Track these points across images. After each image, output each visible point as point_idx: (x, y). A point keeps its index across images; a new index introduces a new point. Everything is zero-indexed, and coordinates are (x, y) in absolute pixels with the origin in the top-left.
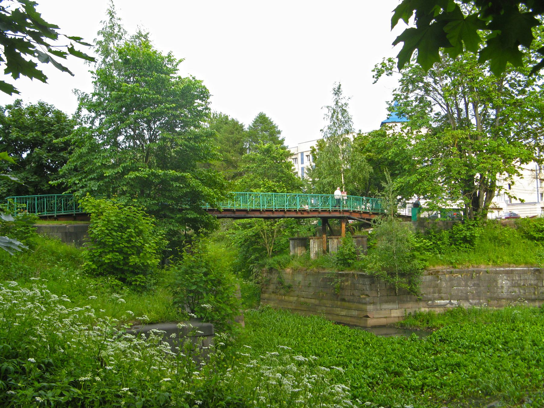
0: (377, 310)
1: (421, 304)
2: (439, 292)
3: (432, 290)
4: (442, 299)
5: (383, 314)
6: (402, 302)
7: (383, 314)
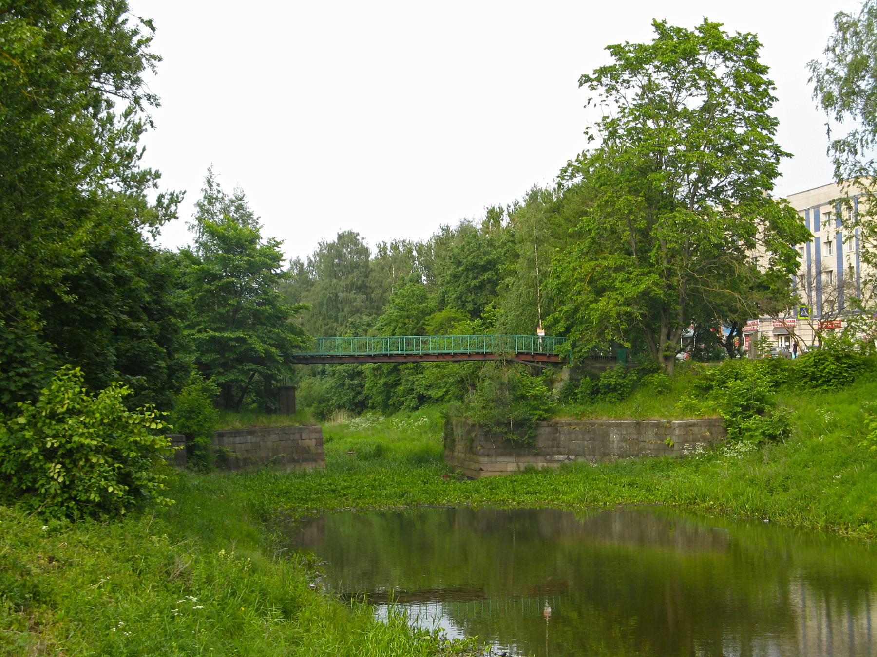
0: (492, 462)
1: (540, 458)
2: (558, 447)
3: (550, 443)
4: (560, 453)
5: (499, 467)
6: (519, 455)
7: (499, 467)
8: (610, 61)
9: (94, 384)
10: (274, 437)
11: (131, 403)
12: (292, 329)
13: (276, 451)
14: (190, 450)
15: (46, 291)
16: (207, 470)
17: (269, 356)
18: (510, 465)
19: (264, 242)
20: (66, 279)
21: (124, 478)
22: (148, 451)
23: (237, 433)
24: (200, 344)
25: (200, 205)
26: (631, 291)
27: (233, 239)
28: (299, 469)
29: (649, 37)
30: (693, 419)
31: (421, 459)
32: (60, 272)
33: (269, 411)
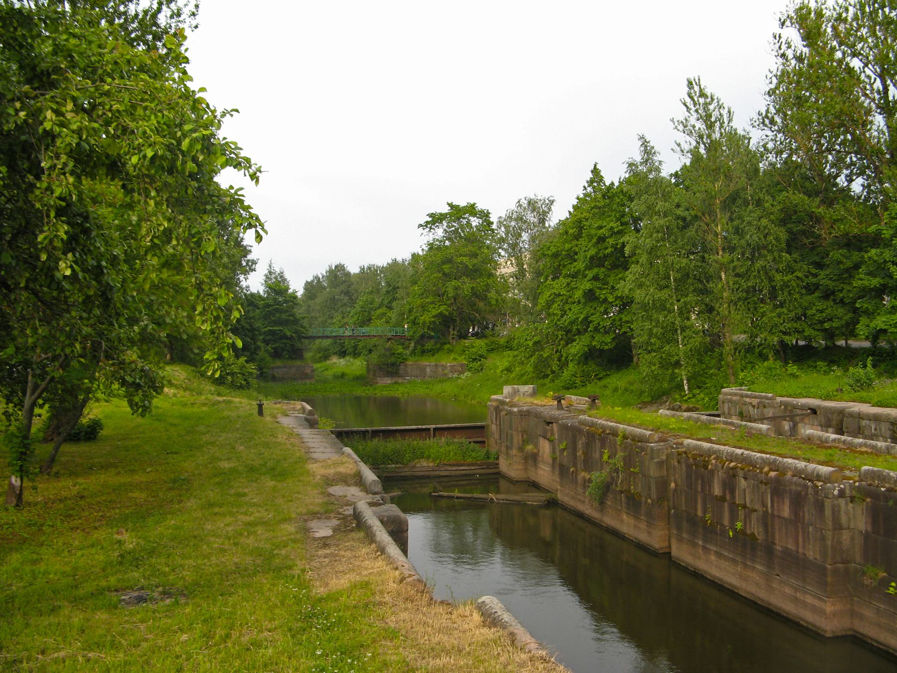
14: (261, 374)
16: (267, 381)
17: (292, 336)
18: (389, 381)
19: (290, 291)
21: (245, 380)
22: (251, 373)
23: (279, 367)
24: (265, 332)
25: (266, 275)
26: (434, 312)
29: (446, 209)
30: (455, 363)
31: (357, 378)
33: (292, 358)
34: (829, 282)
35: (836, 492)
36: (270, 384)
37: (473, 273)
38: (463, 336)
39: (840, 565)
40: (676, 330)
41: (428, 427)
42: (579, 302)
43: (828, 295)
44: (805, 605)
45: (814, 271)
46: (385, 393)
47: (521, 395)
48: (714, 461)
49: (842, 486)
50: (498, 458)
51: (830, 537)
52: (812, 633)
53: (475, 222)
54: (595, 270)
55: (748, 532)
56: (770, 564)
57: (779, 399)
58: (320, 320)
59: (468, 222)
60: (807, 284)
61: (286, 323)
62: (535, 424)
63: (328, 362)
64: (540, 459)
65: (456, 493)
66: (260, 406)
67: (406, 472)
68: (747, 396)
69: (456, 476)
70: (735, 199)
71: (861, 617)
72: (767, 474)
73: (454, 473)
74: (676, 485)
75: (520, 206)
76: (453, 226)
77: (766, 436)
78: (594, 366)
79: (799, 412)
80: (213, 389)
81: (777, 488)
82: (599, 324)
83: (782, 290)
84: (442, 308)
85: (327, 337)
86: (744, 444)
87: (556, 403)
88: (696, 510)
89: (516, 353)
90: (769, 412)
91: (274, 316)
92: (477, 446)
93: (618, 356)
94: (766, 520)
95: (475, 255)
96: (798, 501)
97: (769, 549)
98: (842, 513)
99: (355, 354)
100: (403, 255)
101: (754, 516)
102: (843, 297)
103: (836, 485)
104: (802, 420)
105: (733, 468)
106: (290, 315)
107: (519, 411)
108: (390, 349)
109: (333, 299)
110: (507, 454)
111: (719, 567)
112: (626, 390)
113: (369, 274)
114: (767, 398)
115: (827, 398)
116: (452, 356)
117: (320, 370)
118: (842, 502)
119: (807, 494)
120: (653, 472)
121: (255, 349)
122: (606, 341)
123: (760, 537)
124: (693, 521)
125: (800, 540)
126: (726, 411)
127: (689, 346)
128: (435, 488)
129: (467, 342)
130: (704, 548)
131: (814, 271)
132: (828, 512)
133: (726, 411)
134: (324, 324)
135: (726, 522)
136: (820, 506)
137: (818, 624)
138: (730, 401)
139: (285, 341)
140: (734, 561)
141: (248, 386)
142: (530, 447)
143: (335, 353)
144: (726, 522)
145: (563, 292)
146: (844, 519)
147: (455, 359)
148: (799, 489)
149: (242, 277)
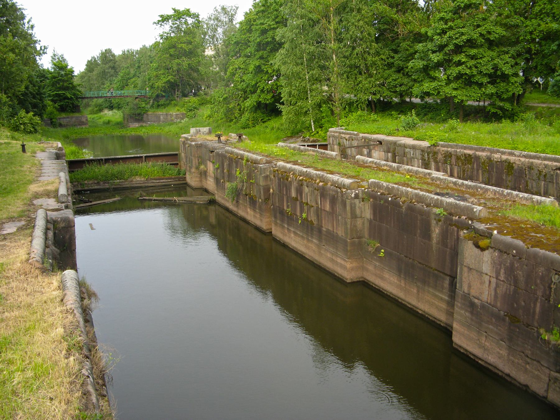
8: (160, 19)
9: (27, 112)
10: (74, 119)
11: (34, 115)
12: (78, 90)
13: (75, 122)
15: (17, 96)
17: (71, 98)
18: (137, 125)
19: (69, 67)
20: (21, 94)
21: (33, 128)
23: (64, 118)
24: (53, 95)
26: (165, 80)
27: (61, 66)
28: (81, 127)
29: (171, 12)
30: (178, 113)
32: (20, 93)
33: (73, 112)
34: (400, 62)
35: (353, 195)
36: (59, 129)
37: (190, 54)
38: (185, 95)
39: (356, 240)
40: (307, 92)
41: (141, 155)
42: (251, 73)
43: (400, 70)
44: (337, 263)
45: (392, 54)
46: (133, 133)
47: (200, 134)
48: (291, 176)
49: (357, 192)
50: (185, 174)
51: (349, 223)
52: (339, 280)
53: (190, 21)
54: (261, 53)
55: (309, 220)
56: (320, 239)
57: (361, 135)
58: (96, 85)
59: (186, 21)
60: (388, 63)
61: (67, 89)
62: (204, 152)
63: (102, 113)
64: (208, 174)
65: (154, 197)
66: (23, 146)
67: (127, 184)
68: (343, 133)
69: (159, 186)
70: (345, 8)
71: (367, 270)
72: (318, 184)
73: (157, 184)
74: (273, 191)
75: (217, 10)
76: (176, 24)
77: (335, 159)
78: (260, 114)
79: (372, 143)
80: (9, 134)
81: (323, 192)
82: (264, 88)
83: (372, 67)
84: (170, 77)
85: (101, 97)
86: (320, 166)
87: (217, 139)
88: (283, 206)
89: (212, 106)
90: (355, 143)
91: (59, 84)
92: (172, 167)
93: (270, 109)
94: (319, 212)
95: (190, 43)
96: (333, 201)
97: (320, 231)
98: (357, 207)
99: (119, 108)
100: (149, 42)
101: (312, 209)
102: (408, 72)
103: (353, 191)
104: (374, 148)
105: (301, 180)
106: (70, 84)
107: (195, 144)
108: (136, 105)
109: (104, 72)
110: (190, 171)
111: (295, 241)
112: (278, 129)
113: (127, 56)
114: (354, 135)
115: (389, 134)
116: (177, 108)
117: (96, 119)
118: (357, 201)
119: (337, 196)
120: (262, 183)
121: (43, 106)
122: (267, 98)
123: (315, 223)
124: (282, 212)
125: (335, 224)
126: (331, 142)
127: (313, 102)
128: (141, 194)
129: (186, 99)
130: (288, 229)
131: (392, 54)
132: (348, 208)
133: (331, 142)
134: (99, 89)
135: (298, 214)
136: (344, 204)
137: (343, 275)
138: (333, 136)
139: (67, 101)
140: (302, 237)
141: (36, 131)
142: (202, 167)
143: (107, 108)
144: (298, 214)
145: (242, 66)
146: (358, 212)
147: (178, 110)
148: (334, 193)
149: (37, 58)
